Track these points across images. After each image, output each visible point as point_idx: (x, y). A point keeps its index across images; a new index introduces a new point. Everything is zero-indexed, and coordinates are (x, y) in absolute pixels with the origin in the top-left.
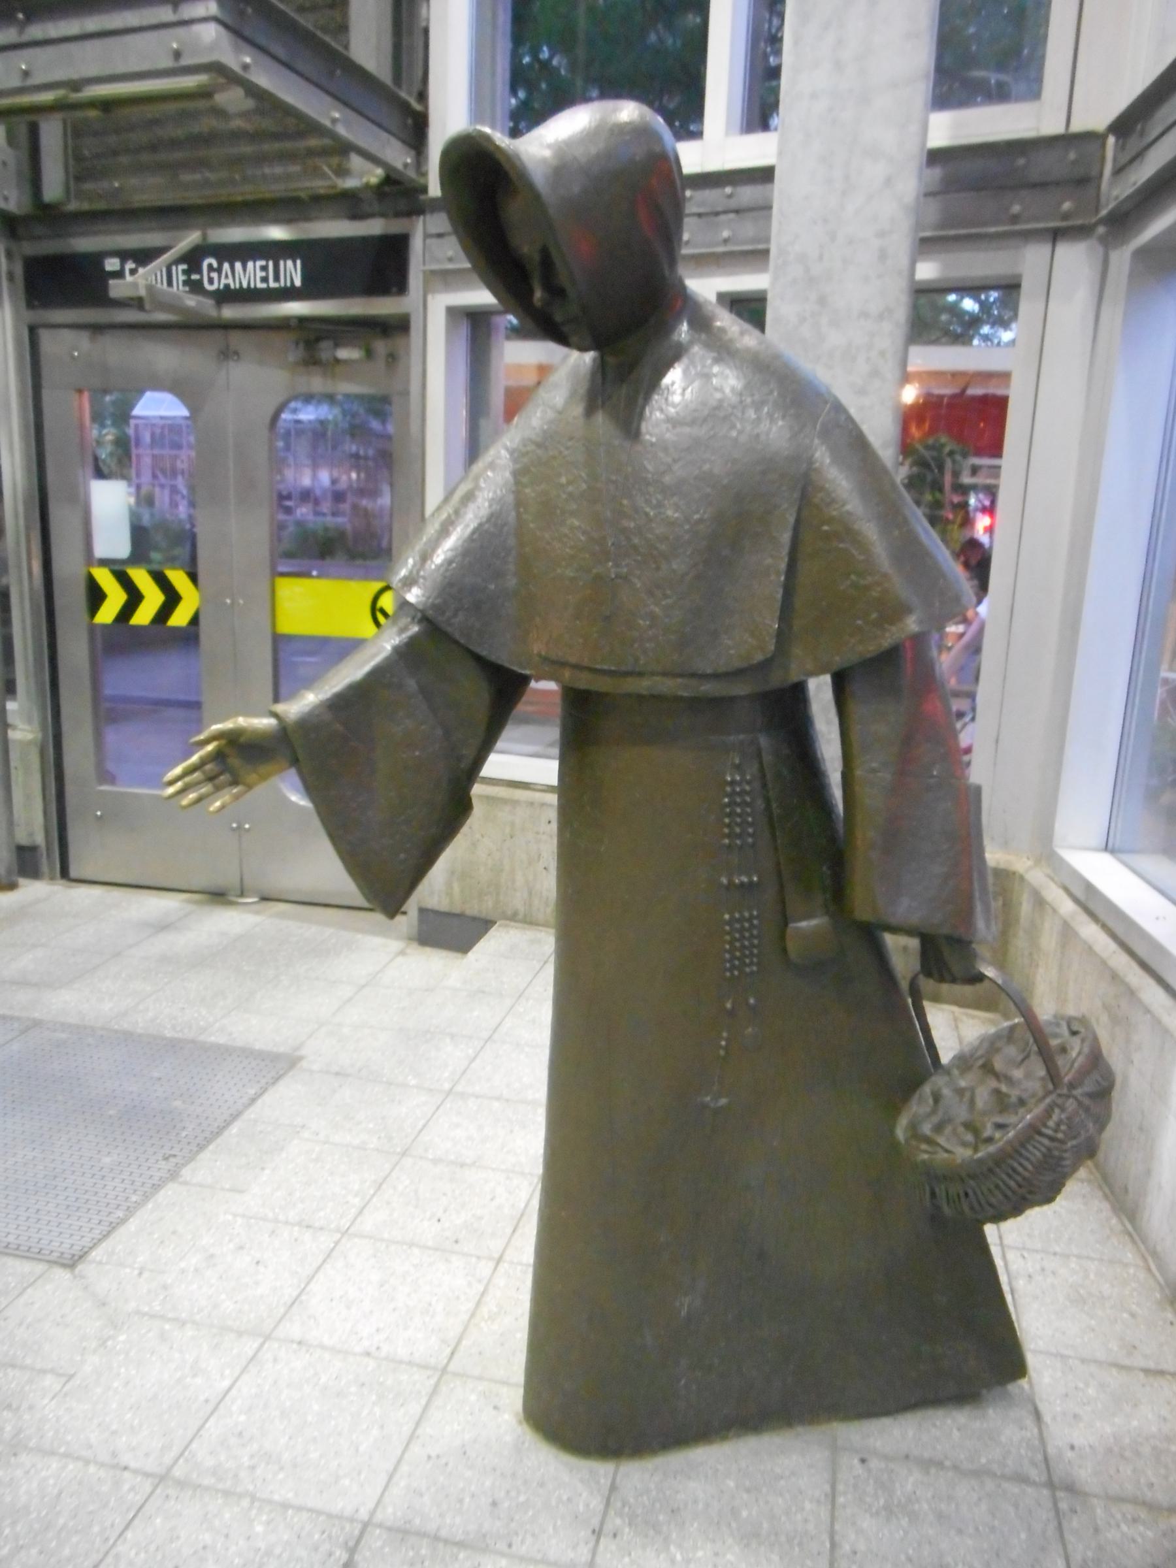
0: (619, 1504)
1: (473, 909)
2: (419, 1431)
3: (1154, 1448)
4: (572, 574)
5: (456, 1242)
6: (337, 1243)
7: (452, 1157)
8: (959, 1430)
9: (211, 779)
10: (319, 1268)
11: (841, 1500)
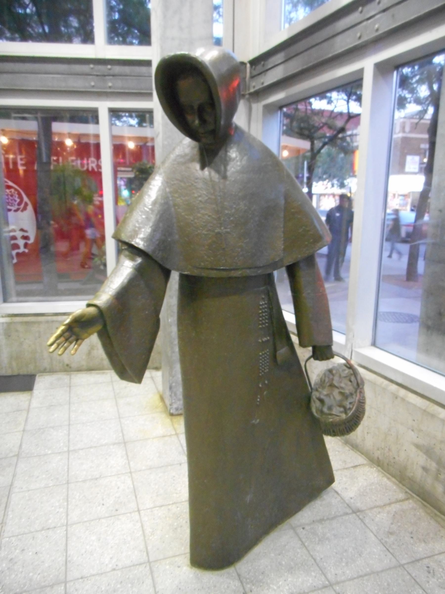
0: (244, 580)
1: (24, 371)
2: (157, 590)
3: (370, 489)
4: (206, 233)
5: (117, 510)
6: (67, 530)
7: (90, 477)
8: (321, 506)
9: (67, 340)
10: (66, 544)
11: (306, 544)
